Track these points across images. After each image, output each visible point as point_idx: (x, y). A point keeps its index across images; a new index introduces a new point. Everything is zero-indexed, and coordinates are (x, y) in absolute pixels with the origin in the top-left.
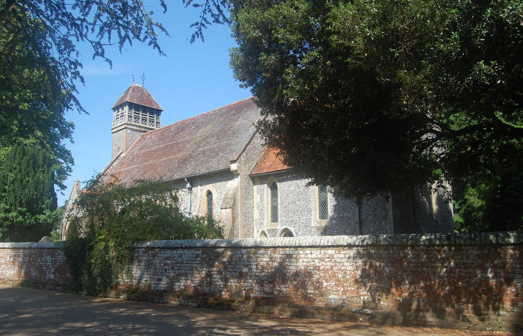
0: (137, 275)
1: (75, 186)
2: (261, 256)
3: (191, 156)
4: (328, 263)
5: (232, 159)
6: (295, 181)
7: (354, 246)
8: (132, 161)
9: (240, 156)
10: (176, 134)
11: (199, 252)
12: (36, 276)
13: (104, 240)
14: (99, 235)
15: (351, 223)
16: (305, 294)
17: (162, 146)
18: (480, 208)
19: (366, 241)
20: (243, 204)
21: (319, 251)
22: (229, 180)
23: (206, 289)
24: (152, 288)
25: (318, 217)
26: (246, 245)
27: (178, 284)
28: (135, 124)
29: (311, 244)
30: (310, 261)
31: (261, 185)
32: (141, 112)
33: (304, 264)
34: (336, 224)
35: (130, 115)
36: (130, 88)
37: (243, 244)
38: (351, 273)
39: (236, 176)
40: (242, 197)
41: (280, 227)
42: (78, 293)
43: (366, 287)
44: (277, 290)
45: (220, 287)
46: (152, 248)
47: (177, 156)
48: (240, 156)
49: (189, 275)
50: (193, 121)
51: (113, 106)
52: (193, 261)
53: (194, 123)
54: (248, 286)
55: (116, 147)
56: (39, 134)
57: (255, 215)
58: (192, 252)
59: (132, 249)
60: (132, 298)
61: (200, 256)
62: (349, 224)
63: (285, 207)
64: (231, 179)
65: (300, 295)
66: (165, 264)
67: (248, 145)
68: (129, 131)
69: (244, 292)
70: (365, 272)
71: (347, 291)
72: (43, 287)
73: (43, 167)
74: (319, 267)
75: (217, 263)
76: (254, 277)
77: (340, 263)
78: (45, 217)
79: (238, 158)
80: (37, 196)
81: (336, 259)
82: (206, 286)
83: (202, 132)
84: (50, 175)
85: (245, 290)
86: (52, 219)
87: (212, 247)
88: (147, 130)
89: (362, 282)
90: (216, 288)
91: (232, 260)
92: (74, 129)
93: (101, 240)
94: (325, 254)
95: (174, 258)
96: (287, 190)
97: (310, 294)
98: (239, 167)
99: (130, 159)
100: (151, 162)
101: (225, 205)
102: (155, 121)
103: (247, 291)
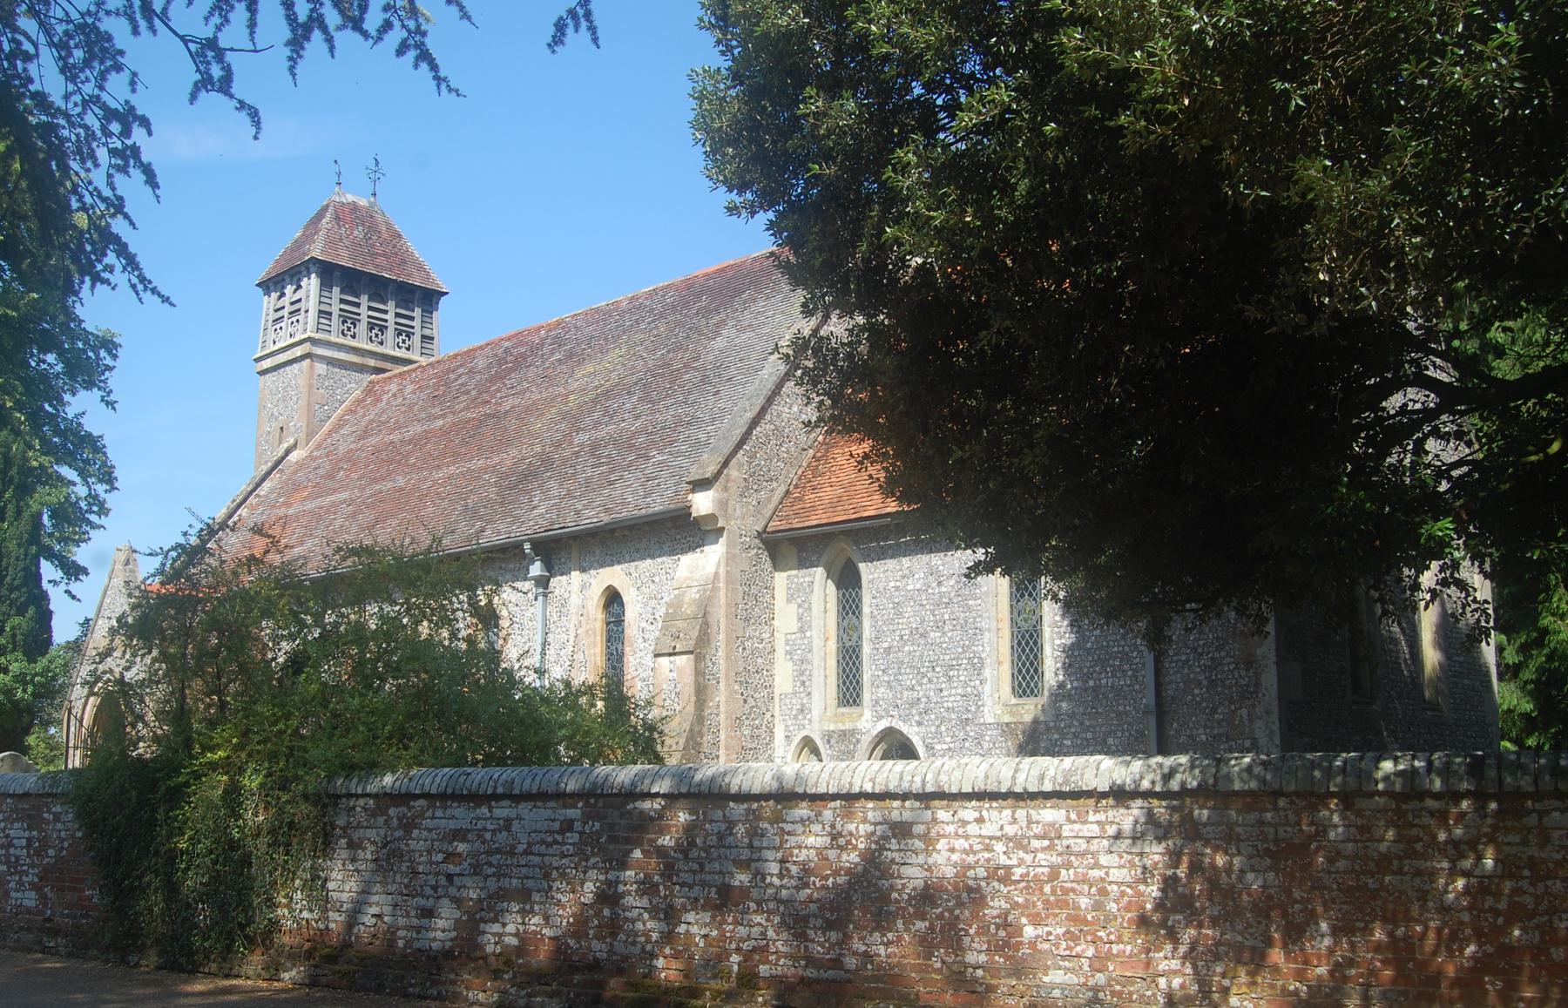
0: (345, 897)
1: (119, 566)
2: (799, 828)
3: (546, 461)
5: (695, 473)
6: (925, 558)
7: (1136, 794)
8: (330, 476)
9: (725, 464)
11: (573, 813)
13: (225, 765)
14: (207, 748)
15: (1126, 713)
16: (955, 968)
19: (1178, 777)
20: (737, 640)
21: (1007, 812)
22: (684, 551)
23: (599, 948)
24: (401, 943)
26: (745, 788)
27: (496, 928)
28: (341, 340)
29: (980, 786)
30: (976, 847)
32: (364, 300)
34: (1072, 716)
35: (324, 307)
36: (327, 206)
37: (736, 784)
38: (1123, 894)
41: (869, 723)
42: (124, 962)
44: (855, 953)
45: (648, 941)
47: (497, 460)
48: (725, 464)
49: (536, 897)
50: (558, 334)
51: (261, 275)
52: (549, 845)
53: (559, 342)
57: (778, 680)
58: (549, 813)
59: (327, 802)
60: (324, 980)
62: (1119, 715)
63: (888, 650)
65: (939, 971)
66: (450, 857)
67: (755, 422)
68: (321, 368)
69: (735, 958)
71: (1110, 956)
74: (1008, 868)
76: (772, 905)
77: (1082, 854)
78: (7, 679)
79: (719, 473)
82: (596, 937)
83: (589, 375)
84: (24, 526)
85: (738, 950)
86: (30, 689)
88: (388, 366)
91: (692, 844)
92: (115, 357)
93: (214, 766)
94: (1030, 822)
96: (897, 588)
97: (975, 968)
98: (723, 504)
99: (322, 472)
100: (401, 482)
102: (418, 331)
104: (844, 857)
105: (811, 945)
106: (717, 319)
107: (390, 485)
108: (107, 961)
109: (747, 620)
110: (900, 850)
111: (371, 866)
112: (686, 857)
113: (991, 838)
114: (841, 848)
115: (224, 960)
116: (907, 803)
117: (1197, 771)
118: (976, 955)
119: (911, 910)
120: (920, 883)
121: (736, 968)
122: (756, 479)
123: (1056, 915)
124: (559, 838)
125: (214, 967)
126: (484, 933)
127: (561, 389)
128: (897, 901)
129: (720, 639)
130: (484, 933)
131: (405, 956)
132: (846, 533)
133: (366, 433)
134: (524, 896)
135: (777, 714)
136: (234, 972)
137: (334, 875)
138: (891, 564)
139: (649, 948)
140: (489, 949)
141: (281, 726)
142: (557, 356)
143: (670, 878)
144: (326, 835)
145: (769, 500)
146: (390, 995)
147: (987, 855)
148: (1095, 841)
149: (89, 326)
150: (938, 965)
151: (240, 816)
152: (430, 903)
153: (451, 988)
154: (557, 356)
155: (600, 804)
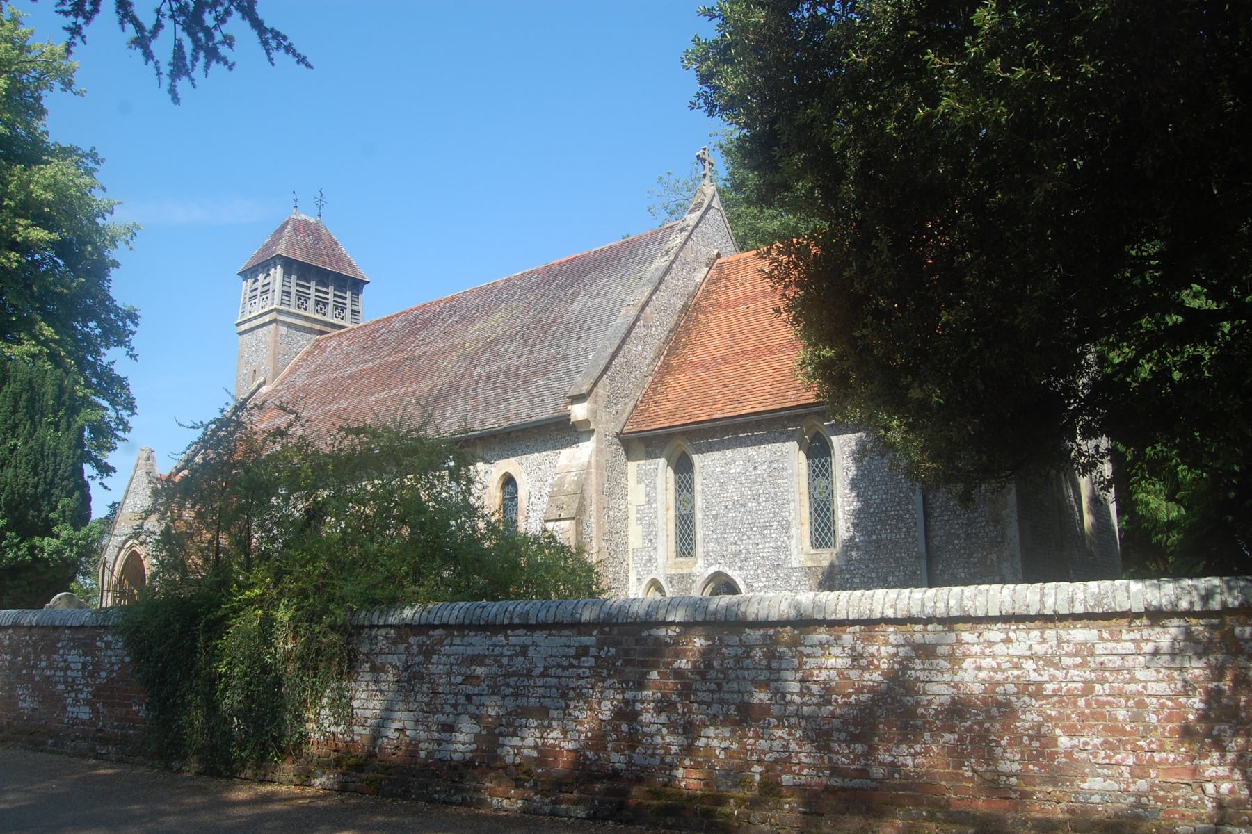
0: (368, 713)
1: (142, 462)
2: (819, 651)
3: (453, 387)
4: (1072, 672)
5: (574, 391)
6: (744, 450)
7: (1175, 613)
9: (595, 384)
10: (407, 336)
11: (587, 640)
12: (34, 710)
13: (260, 601)
14: (243, 587)
15: (902, 558)
16: (988, 776)
17: (370, 364)
18: (1171, 525)
19: (1218, 598)
20: (604, 510)
21: (1035, 634)
22: (563, 447)
23: (617, 760)
24: (423, 754)
25: (807, 542)
26: (762, 615)
27: (516, 741)
28: (297, 311)
29: (1007, 609)
30: (1004, 666)
31: (649, 462)
32: (313, 285)
33: (982, 675)
34: (860, 561)
35: (286, 289)
36: (287, 223)
37: (752, 612)
38: (1163, 706)
39: (584, 436)
40: (600, 492)
41: (701, 568)
42: (170, 769)
43: (1223, 750)
44: (881, 764)
45: (668, 752)
46: (420, 626)
47: (415, 387)
48: (595, 384)
49: (554, 714)
50: (453, 305)
51: (242, 268)
52: (565, 668)
53: (454, 310)
54: (771, 750)
55: (247, 370)
56: (48, 331)
57: (631, 539)
58: (564, 640)
59: (352, 631)
60: (352, 786)
61: (593, 651)
62: (897, 560)
63: (716, 517)
64: (569, 444)
65: (971, 779)
66: (468, 679)
67: (614, 356)
68: (283, 330)
69: (757, 769)
70: (1219, 702)
71: (1151, 764)
72: (55, 745)
73: (55, 413)
74: (1039, 685)
75: (654, 675)
76: (793, 721)
77: (1118, 670)
78: (59, 542)
79: (591, 390)
80: (36, 486)
81: (1105, 659)
82: (614, 750)
83: (478, 331)
84: (72, 435)
85: (760, 761)
86: (75, 549)
87: (634, 623)
88: (329, 329)
89: (1209, 734)
90: (653, 756)
91: (709, 666)
92: (136, 325)
93: (250, 602)
94: (1060, 641)
95: (497, 659)
96: (722, 472)
97: (1009, 775)
98: (594, 412)
100: (344, 404)
101: (554, 513)
102: (349, 306)
103: (770, 767)
104: (867, 676)
105: (835, 757)
106: (572, 291)
107: (336, 406)
108: (153, 767)
109: (610, 495)
110: (925, 670)
111: (394, 687)
112: (704, 679)
113: (1019, 657)
114: (863, 669)
115: (259, 768)
116: (930, 627)
117: (1236, 593)
118: (1010, 764)
119: (939, 724)
120: (946, 700)
121: (757, 777)
122: (616, 396)
123: (1092, 727)
124: (575, 662)
125: (249, 773)
126: (503, 745)
127: (459, 340)
128: (923, 716)
129: (592, 509)
130: (503, 745)
131: (427, 765)
132: (683, 433)
133: (315, 373)
134: (542, 713)
135: (630, 562)
136: (268, 778)
137: (358, 694)
138: (717, 455)
139: (668, 759)
140: (509, 760)
141: (310, 567)
142: (454, 319)
143: (688, 697)
144: (350, 661)
145: (624, 410)
146: (416, 800)
147: (1016, 672)
148: (1131, 658)
149: (119, 304)
150: (969, 774)
151: (272, 644)
152: (450, 719)
153: (476, 796)
154: (454, 319)
155: (615, 632)
